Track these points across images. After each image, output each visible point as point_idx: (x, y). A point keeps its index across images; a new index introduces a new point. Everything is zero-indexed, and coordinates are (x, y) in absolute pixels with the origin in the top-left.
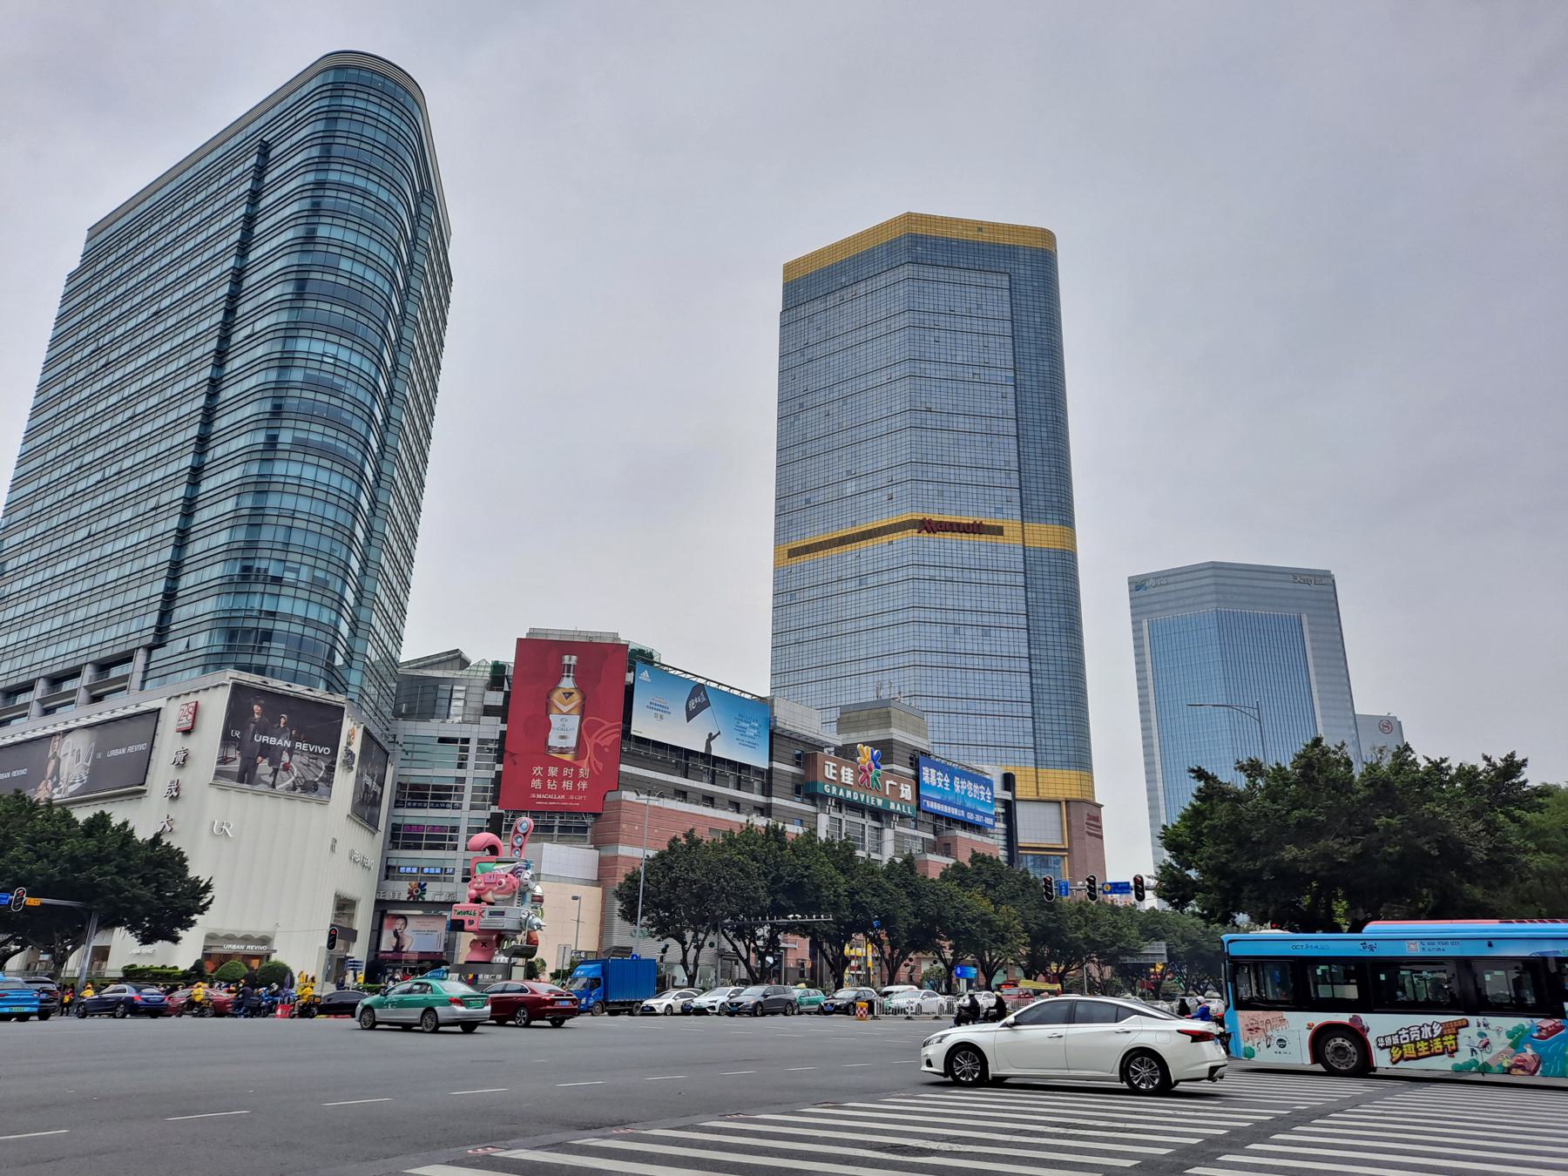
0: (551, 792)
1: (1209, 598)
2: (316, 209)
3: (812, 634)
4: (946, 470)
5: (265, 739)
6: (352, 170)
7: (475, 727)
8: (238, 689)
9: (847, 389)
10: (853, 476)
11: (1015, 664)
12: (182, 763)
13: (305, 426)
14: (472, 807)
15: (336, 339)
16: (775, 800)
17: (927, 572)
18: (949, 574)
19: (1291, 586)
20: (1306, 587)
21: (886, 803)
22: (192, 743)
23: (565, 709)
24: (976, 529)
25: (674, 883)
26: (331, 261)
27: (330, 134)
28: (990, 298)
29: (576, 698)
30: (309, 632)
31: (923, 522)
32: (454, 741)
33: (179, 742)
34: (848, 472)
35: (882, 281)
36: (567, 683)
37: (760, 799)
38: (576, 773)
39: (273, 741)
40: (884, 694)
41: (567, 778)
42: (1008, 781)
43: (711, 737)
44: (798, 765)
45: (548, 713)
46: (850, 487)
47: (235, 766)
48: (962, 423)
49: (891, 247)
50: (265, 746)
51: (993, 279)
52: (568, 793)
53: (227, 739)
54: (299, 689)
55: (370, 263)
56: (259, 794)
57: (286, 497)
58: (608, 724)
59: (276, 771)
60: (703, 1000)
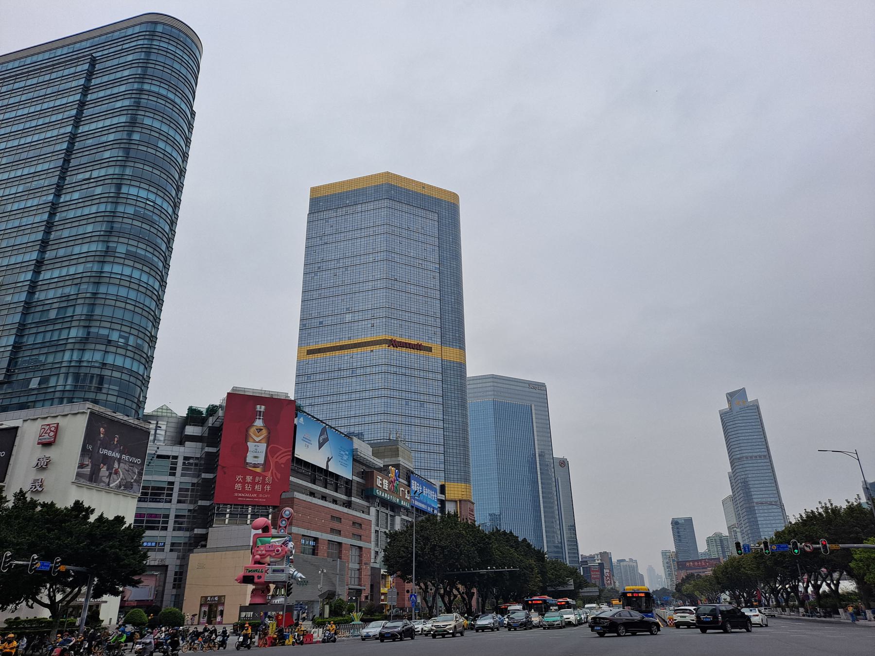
0: (249, 492)
1: (490, 393)
2: (138, 105)
3: (321, 400)
4: (404, 313)
5: (105, 451)
6: (158, 83)
7: (182, 449)
8: (93, 414)
9: (348, 262)
10: (348, 311)
11: (435, 423)
12: (43, 466)
13: (135, 243)
14: (179, 502)
15: (155, 190)
16: (353, 499)
17: (393, 369)
18: (404, 371)
19: (527, 389)
20: (534, 390)
21: (400, 501)
22: (52, 453)
23: (257, 439)
24: (418, 347)
25: (433, 548)
26: (153, 140)
27: (147, 61)
28: (429, 223)
29: (264, 433)
30: (132, 379)
31: (391, 340)
32: (168, 457)
33: (40, 452)
34: (348, 309)
35: (371, 206)
36: (259, 423)
37: (344, 497)
38: (264, 479)
39: (110, 453)
40: (393, 437)
41: (258, 483)
42: (443, 489)
43: (329, 460)
44: (362, 478)
45: (246, 441)
46: (348, 317)
47: (87, 470)
48: (413, 289)
49: (377, 188)
50: (105, 456)
51: (430, 215)
52: (258, 493)
53: (84, 451)
54: (120, 416)
55: (169, 141)
56: (99, 490)
57: (121, 288)
58: (284, 450)
59: (110, 474)
60: (481, 622)
